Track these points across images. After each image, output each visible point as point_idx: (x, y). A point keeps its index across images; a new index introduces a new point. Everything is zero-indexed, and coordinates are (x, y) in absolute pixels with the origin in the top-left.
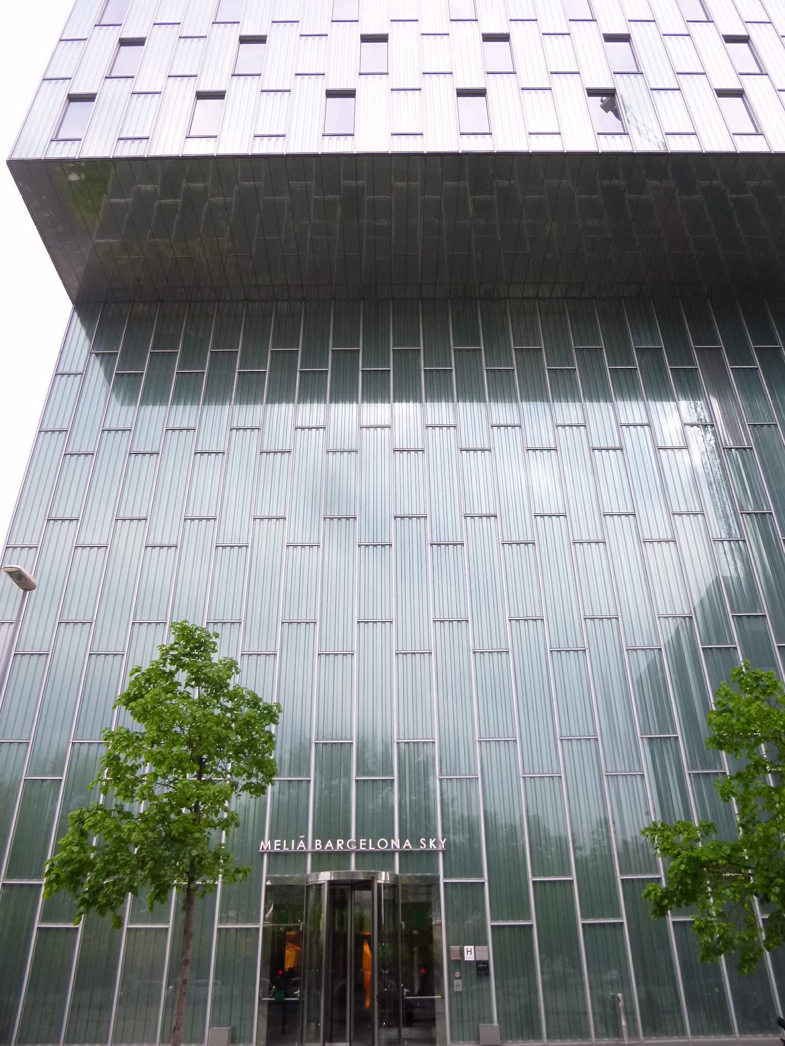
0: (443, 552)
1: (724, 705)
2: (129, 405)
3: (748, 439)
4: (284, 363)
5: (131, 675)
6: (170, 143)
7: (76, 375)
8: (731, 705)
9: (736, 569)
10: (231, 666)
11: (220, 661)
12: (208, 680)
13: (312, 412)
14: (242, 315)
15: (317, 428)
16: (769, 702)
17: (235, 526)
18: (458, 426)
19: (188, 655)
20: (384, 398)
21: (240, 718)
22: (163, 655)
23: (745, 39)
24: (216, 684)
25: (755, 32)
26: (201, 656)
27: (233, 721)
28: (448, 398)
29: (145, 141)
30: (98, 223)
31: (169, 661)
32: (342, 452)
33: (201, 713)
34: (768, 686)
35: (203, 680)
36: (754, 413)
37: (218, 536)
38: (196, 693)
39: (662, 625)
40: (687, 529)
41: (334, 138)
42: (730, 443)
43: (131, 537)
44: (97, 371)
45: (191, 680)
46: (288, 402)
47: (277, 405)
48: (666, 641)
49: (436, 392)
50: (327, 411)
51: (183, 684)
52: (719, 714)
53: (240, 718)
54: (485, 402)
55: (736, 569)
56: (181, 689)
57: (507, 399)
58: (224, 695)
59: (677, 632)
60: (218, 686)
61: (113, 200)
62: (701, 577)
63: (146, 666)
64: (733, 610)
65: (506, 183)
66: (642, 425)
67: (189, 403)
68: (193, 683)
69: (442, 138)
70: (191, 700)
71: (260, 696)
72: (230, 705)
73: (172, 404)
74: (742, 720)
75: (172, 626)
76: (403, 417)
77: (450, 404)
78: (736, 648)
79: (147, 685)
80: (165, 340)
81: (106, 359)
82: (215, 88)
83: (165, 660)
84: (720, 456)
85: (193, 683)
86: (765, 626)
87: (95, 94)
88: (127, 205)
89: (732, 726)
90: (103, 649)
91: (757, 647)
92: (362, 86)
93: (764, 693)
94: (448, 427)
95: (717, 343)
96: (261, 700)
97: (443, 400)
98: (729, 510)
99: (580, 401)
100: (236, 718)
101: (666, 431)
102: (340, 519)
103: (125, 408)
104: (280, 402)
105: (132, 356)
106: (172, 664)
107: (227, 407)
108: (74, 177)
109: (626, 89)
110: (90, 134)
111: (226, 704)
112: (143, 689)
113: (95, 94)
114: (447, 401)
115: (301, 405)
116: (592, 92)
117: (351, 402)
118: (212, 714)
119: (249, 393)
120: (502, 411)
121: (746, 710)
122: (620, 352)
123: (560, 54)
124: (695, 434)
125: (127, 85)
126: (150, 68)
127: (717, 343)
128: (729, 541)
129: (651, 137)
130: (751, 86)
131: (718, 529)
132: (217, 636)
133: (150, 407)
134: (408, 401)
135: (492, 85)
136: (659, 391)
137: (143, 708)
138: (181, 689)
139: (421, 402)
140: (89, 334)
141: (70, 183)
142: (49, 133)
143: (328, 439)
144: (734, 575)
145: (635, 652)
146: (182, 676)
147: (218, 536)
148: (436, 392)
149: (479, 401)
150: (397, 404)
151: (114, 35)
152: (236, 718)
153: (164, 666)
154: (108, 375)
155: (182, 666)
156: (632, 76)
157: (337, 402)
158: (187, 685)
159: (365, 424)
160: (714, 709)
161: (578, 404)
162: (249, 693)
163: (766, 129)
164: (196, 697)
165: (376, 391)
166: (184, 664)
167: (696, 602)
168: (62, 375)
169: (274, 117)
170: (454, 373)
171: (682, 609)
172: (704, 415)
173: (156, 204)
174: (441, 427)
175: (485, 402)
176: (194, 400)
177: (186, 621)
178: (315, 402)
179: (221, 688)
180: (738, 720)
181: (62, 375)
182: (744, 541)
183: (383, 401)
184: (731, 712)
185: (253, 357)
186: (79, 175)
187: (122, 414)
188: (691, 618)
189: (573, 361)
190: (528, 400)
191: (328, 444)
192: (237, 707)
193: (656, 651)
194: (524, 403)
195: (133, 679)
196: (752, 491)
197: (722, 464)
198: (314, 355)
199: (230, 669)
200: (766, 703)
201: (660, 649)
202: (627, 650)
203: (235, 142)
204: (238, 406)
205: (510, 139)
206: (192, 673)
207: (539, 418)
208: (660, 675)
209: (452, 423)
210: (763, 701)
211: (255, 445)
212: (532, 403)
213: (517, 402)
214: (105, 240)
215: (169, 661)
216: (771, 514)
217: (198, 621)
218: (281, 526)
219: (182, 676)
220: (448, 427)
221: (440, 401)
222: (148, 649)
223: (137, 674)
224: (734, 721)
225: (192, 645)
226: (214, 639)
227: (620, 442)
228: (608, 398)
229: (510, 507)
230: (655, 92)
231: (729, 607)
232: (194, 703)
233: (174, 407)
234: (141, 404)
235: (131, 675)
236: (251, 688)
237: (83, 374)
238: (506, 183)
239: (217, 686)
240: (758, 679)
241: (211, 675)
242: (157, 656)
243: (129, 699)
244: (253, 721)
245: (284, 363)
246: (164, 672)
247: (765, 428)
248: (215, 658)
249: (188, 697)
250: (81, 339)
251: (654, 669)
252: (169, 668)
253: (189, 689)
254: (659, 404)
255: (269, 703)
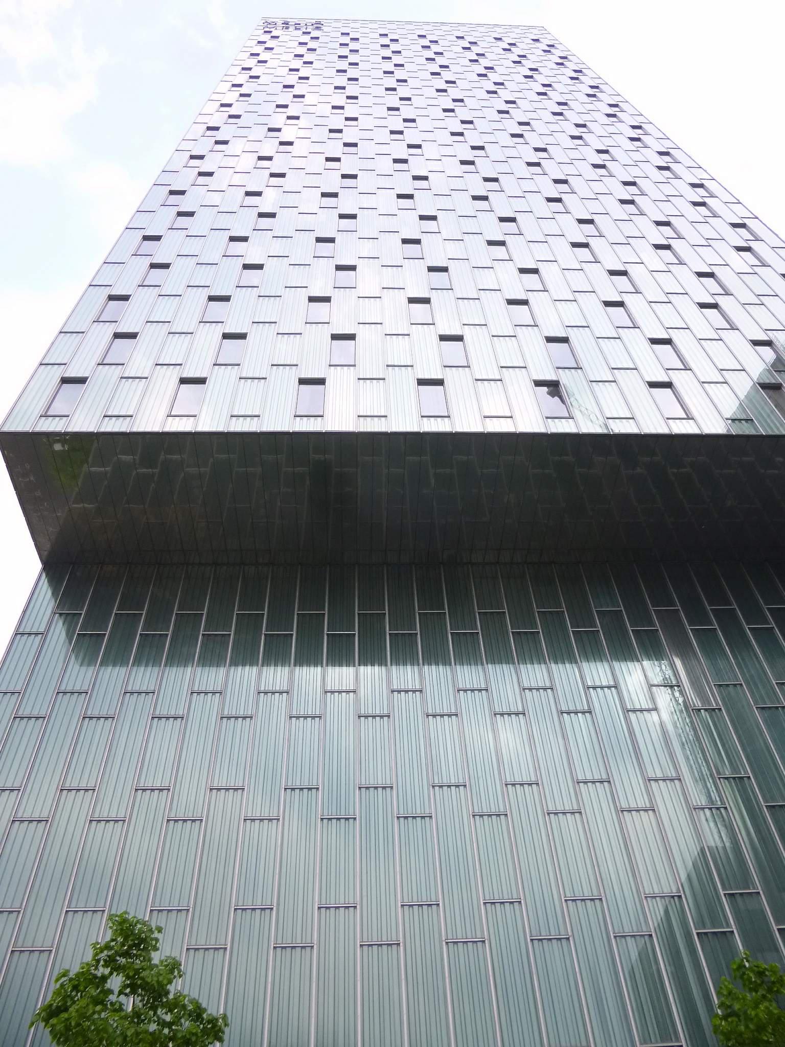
0: (411, 825)
1: (730, 1007)
2: (89, 665)
3: (716, 700)
4: (249, 625)
5: (57, 980)
6: (152, 420)
7: (37, 634)
8: (737, 1007)
9: (721, 837)
10: (173, 967)
11: (162, 962)
12: (146, 986)
13: (276, 676)
14: (209, 578)
15: (281, 693)
16: (777, 1002)
17: (190, 797)
18: (424, 691)
19: (126, 954)
20: (349, 662)
21: (179, 1035)
22: (97, 954)
23: (668, 342)
24: (154, 991)
25: (675, 336)
26: (140, 956)
27: (171, 1039)
28: (414, 661)
29: (129, 419)
30: (77, 489)
31: (102, 963)
32: (305, 718)
33: (133, 1030)
34: (774, 983)
35: (140, 986)
36: (718, 673)
37: (171, 809)
38: (129, 1004)
39: (649, 905)
40: (665, 795)
41: (305, 419)
42: (698, 704)
43: (77, 808)
44: (59, 630)
45: (126, 986)
46: (251, 665)
47: (240, 668)
48: (656, 925)
49: (401, 657)
50: (292, 673)
51: (116, 992)
52: (725, 1017)
53: (179, 1035)
54: (450, 665)
55: (721, 837)
56: (113, 998)
57: (472, 662)
58: (163, 1006)
59: (666, 912)
60: (156, 994)
61: (93, 469)
62: (685, 850)
63: (75, 969)
64: (724, 888)
65: (465, 458)
66: (609, 687)
67: (151, 665)
68: (128, 990)
69: (404, 420)
70: (123, 1014)
71: (204, 1005)
72: (168, 1018)
73: (133, 665)
74: (752, 1026)
75: (111, 918)
76: (368, 680)
77: (416, 668)
78: (733, 932)
79: (74, 993)
80: (132, 601)
81: (70, 619)
82: (197, 375)
83: (98, 961)
84: (690, 716)
85: (128, 990)
86: (760, 903)
87: (87, 378)
88: (106, 473)
89: (741, 1034)
90: (28, 946)
91: (758, 938)
92: (332, 376)
93: (770, 990)
94: (414, 691)
95: (674, 605)
96: (205, 1010)
97: (409, 664)
98: (705, 770)
99: (545, 663)
100: (175, 1035)
101: (631, 689)
102: (302, 789)
103: (84, 669)
104: (244, 665)
105: (96, 618)
106: (106, 966)
107: (189, 669)
108: (58, 447)
109: (565, 378)
110: (78, 412)
111: (164, 1017)
112: (69, 1000)
113: (87, 378)
114: (412, 664)
115: (265, 668)
116: (538, 383)
117: (316, 665)
118: (147, 1032)
119: (213, 656)
120: (468, 675)
121: (753, 1013)
122: (582, 617)
123: (508, 352)
124: (664, 698)
125: (117, 371)
126: (138, 357)
127: (674, 605)
128: (710, 809)
129: (594, 419)
130: (678, 378)
131: (699, 799)
132: (160, 930)
133: (110, 668)
134: (373, 665)
135: (450, 377)
136: (623, 652)
137: (66, 1026)
138: (113, 998)
139: (386, 665)
140: (55, 594)
141: (54, 452)
142: (39, 408)
143: (291, 704)
144: (720, 845)
145: (623, 940)
146: (116, 982)
147: (171, 809)
148: (401, 657)
149: (445, 664)
150: (362, 668)
151: (111, 329)
152: (175, 1035)
153: (96, 968)
154: (69, 635)
155: (117, 969)
156: (573, 370)
157: (301, 665)
158: (120, 993)
159: (329, 688)
160: (719, 1012)
161: (543, 666)
162: (191, 1002)
163: (695, 413)
164: (130, 1009)
165: (340, 654)
166: (120, 966)
167: (684, 877)
168: (23, 634)
169: (253, 399)
170: (419, 636)
171: (669, 887)
172: (669, 673)
173: (135, 472)
174: (407, 692)
175: (450, 665)
176: (156, 662)
177: (126, 913)
178: (280, 664)
179: (160, 996)
180: (747, 1027)
181: (23, 634)
182: (726, 808)
183: (348, 665)
184: (738, 1016)
185: (218, 619)
186: (63, 446)
187: (80, 675)
188: (680, 897)
189: (536, 623)
190: (493, 662)
191: (291, 709)
192: (176, 1021)
193: (646, 937)
194: (490, 666)
195: (58, 986)
196: (723, 745)
197: (692, 722)
198: (280, 619)
199: (172, 972)
200: (774, 1004)
201: (651, 936)
202: (615, 937)
203: (210, 420)
204: (200, 669)
205: (467, 421)
206: (128, 977)
207: (506, 681)
208: (654, 968)
209: (418, 687)
210: (770, 1001)
211: (216, 709)
212: (497, 666)
213: (482, 664)
214: (81, 505)
215: (102, 963)
216: (749, 777)
217: (139, 912)
218: (239, 797)
219: (116, 982)
220: (414, 691)
221: (405, 664)
222: (80, 943)
223: (63, 979)
224: (742, 1028)
225: (131, 941)
226: (156, 935)
227: (589, 706)
228: (572, 660)
229: (480, 774)
230: (594, 384)
231: (718, 876)
232: (126, 1017)
233: (135, 668)
234: (101, 665)
235: (57, 980)
236: (194, 995)
237: (44, 635)
238: (465, 458)
239: (155, 993)
240: (761, 974)
241: (149, 980)
242: (89, 957)
243: (51, 1013)
244: (194, 1039)
245: (249, 625)
246: (95, 977)
247: (731, 688)
248: (156, 957)
249: (121, 1009)
250: (47, 599)
251: (646, 958)
252: (102, 971)
253: (122, 998)
254: (623, 665)
255: (215, 1014)
